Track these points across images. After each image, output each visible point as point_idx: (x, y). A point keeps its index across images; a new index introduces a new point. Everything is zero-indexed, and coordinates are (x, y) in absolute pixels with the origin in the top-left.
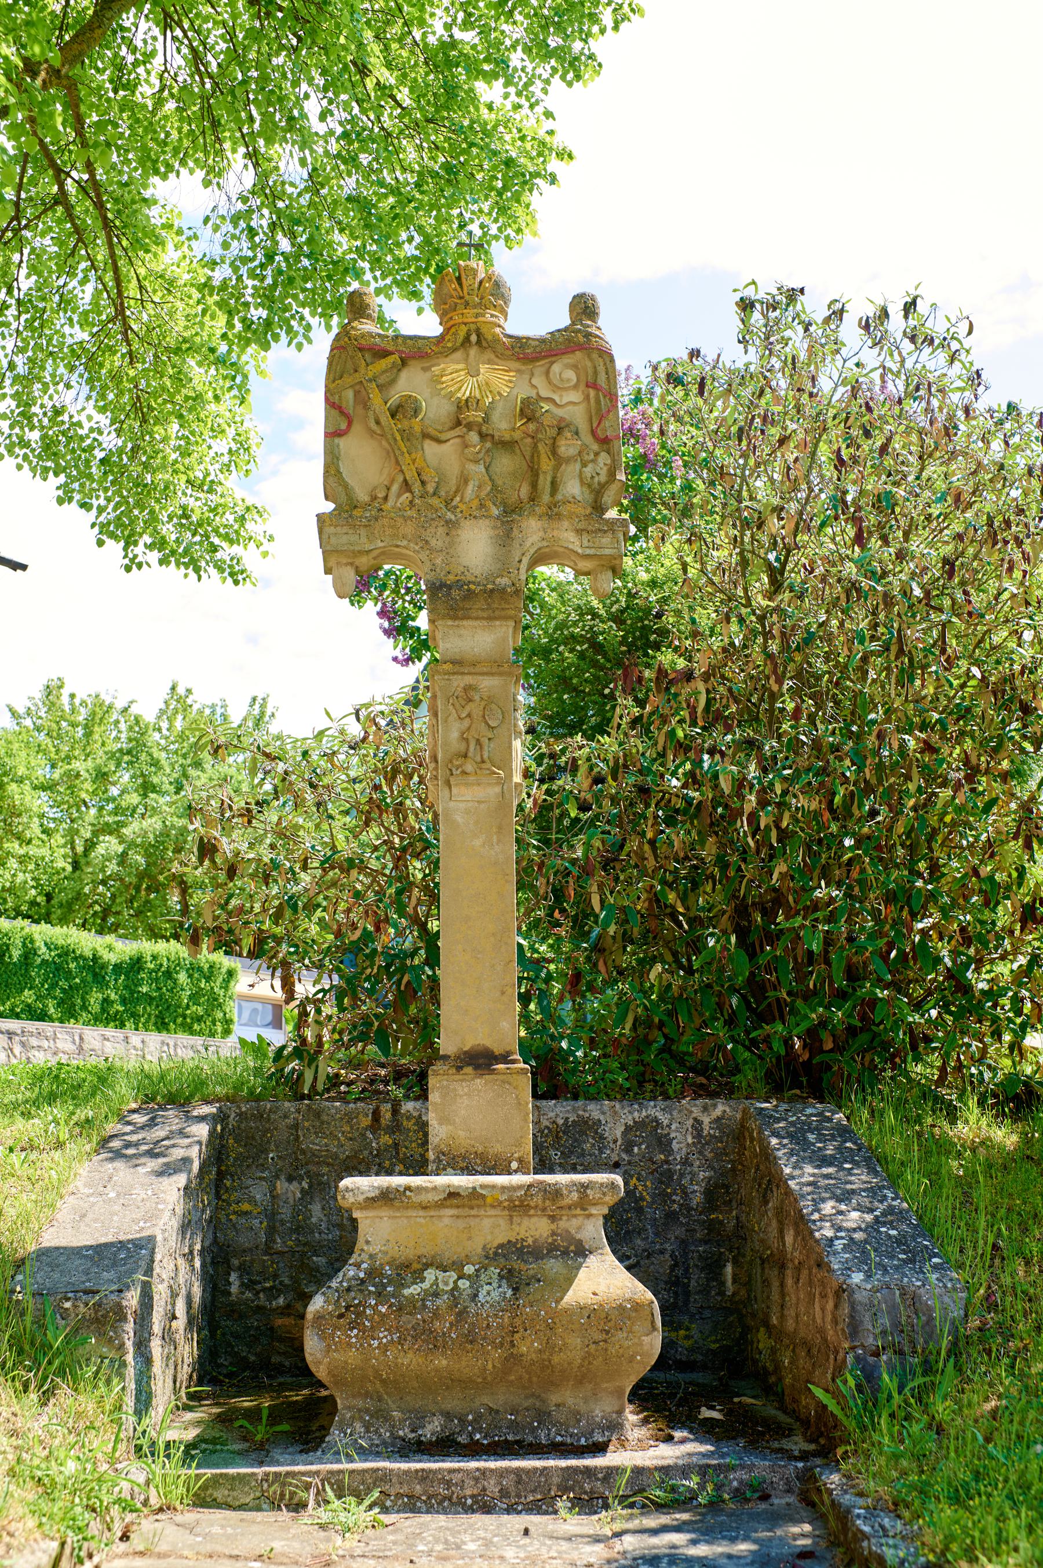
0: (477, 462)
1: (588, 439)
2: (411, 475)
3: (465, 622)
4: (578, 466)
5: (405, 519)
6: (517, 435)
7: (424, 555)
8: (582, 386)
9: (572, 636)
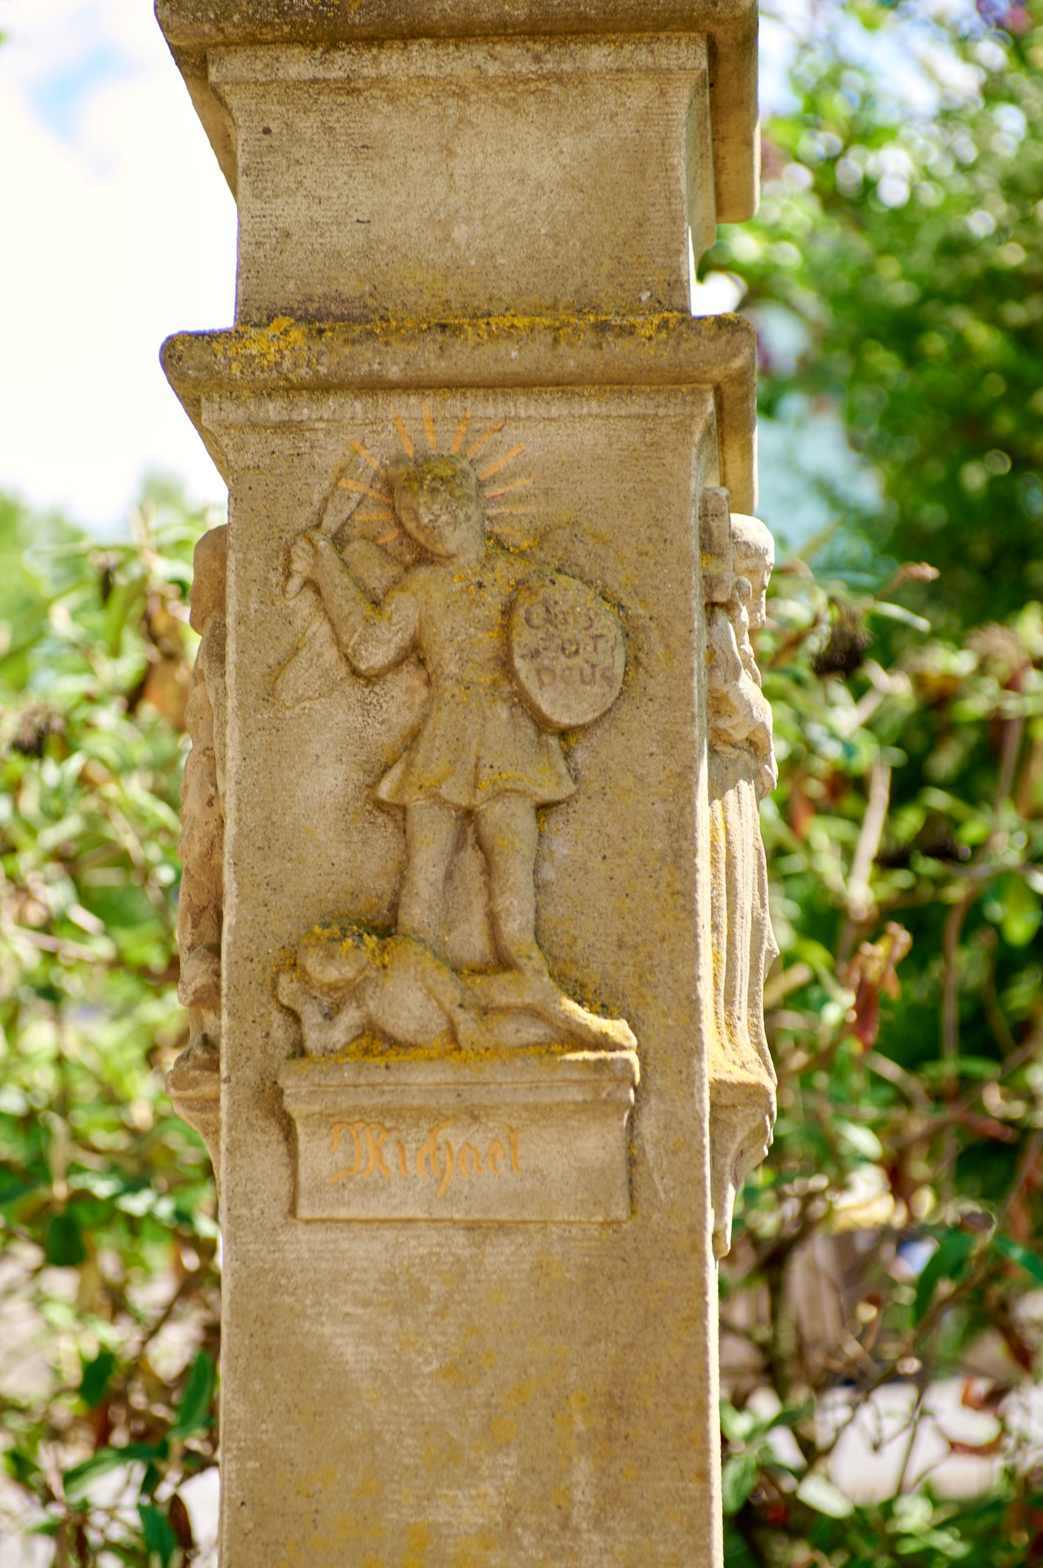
3: (392, 63)
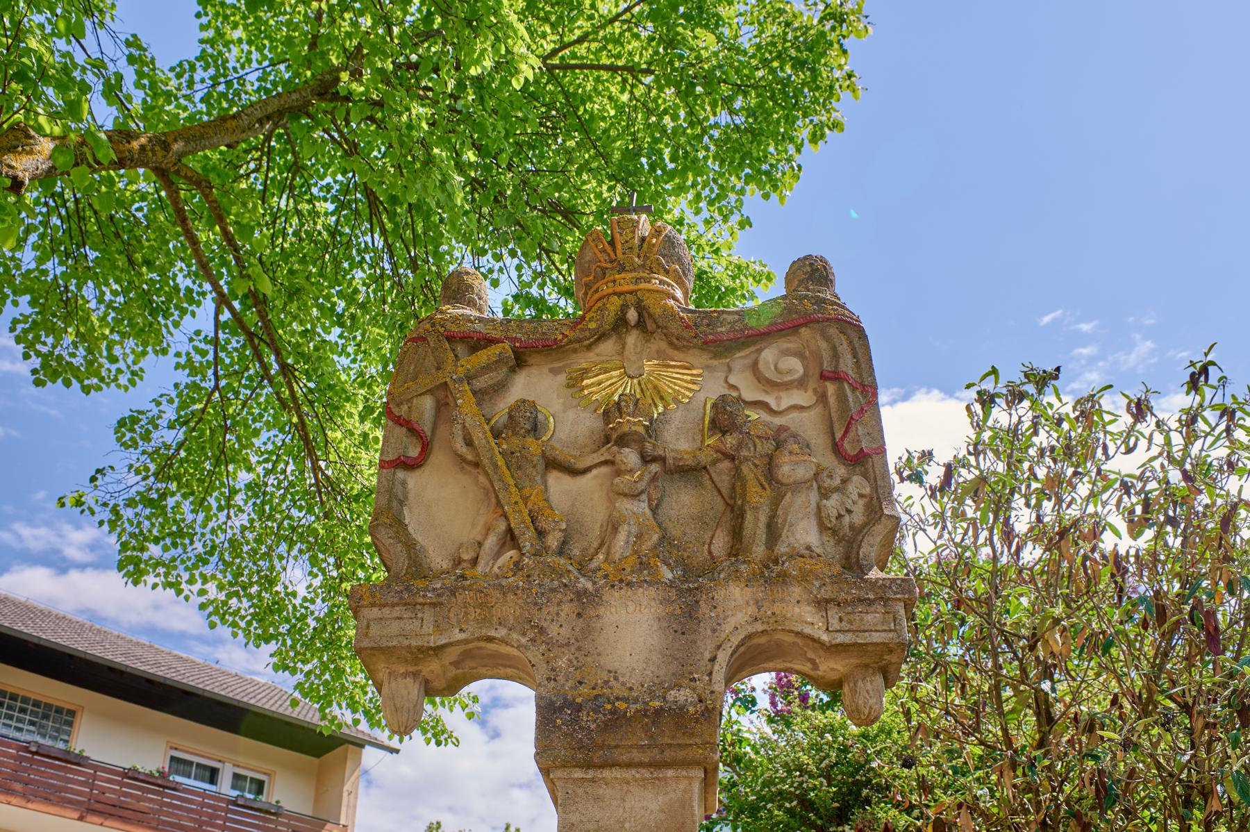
0: (635, 496)
1: (829, 460)
2: (519, 520)
3: (606, 773)
4: (814, 497)
6: (705, 458)
7: (534, 654)
8: (813, 383)
9: (780, 793)
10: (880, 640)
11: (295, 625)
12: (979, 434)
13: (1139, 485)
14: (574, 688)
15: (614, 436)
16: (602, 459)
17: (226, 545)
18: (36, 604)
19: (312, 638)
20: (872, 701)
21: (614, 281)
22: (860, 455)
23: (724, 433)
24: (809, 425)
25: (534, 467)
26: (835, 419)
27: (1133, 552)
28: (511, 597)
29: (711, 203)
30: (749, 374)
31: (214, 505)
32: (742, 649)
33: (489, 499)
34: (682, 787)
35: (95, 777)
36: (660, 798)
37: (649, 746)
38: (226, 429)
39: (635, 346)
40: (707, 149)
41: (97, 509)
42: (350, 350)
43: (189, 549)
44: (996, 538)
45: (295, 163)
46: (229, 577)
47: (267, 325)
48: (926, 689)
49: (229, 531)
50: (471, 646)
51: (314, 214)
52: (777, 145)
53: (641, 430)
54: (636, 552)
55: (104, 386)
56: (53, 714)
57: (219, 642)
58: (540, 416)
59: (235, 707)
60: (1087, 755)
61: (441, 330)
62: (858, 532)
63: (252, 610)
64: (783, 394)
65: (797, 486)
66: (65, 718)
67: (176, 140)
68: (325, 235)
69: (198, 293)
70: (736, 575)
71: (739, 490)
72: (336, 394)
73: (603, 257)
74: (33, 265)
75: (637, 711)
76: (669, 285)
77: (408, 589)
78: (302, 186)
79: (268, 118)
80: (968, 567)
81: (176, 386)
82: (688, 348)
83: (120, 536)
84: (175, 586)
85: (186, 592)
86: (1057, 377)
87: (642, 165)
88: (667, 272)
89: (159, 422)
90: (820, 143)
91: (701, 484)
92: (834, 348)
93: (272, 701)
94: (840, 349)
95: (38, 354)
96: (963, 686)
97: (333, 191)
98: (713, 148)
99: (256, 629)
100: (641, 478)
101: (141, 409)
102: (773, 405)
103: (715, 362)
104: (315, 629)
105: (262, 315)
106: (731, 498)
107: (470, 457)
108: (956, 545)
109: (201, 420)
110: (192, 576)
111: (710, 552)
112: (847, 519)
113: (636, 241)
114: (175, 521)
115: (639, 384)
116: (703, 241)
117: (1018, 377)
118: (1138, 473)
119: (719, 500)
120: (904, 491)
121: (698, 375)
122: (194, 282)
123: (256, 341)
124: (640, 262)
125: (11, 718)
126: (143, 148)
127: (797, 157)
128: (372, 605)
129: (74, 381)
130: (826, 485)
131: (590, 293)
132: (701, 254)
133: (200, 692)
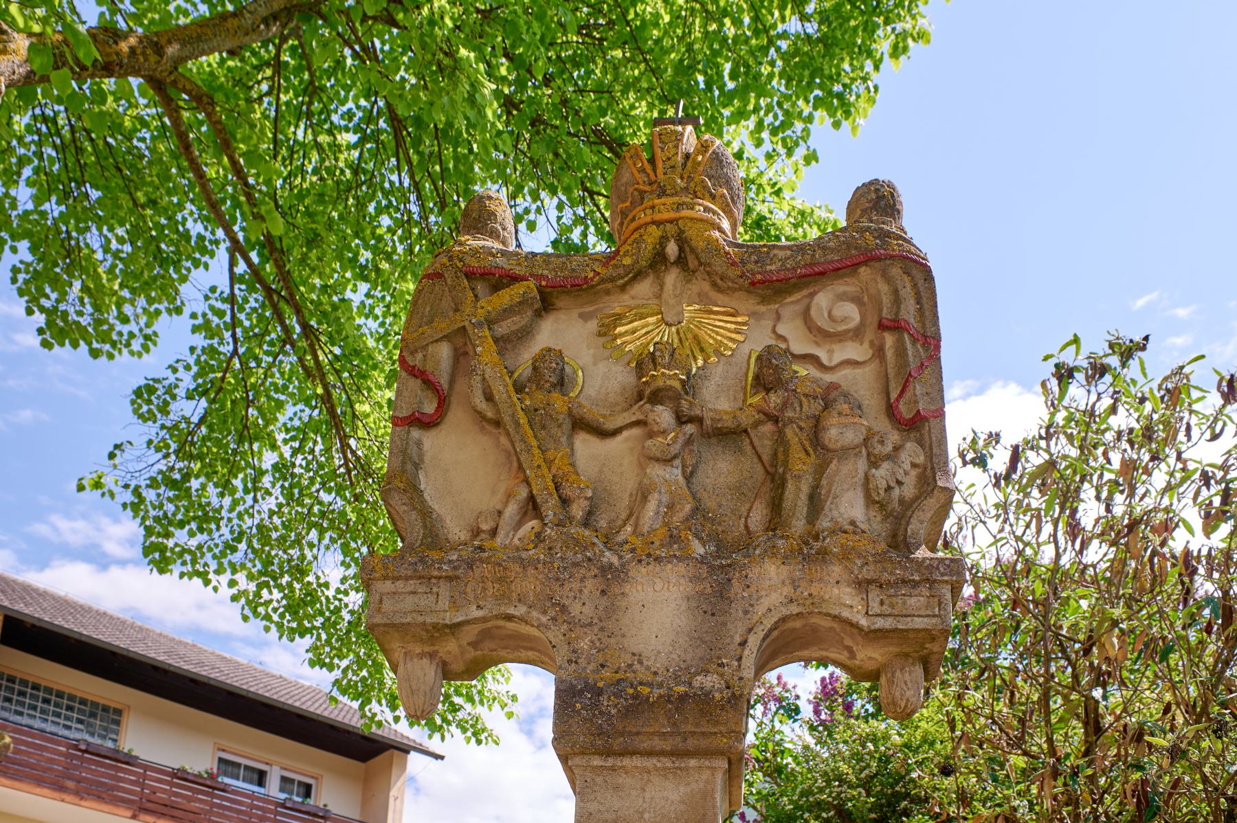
0: (668, 461)
1: (882, 424)
2: (542, 486)
3: (627, 762)
4: (862, 465)
5: (524, 564)
6: (746, 419)
7: (555, 635)
8: (870, 334)
9: (819, 804)
10: (922, 626)
11: (329, 619)
12: (1053, 415)
13: (1220, 474)
14: (596, 671)
15: (647, 392)
16: (634, 419)
17: (254, 530)
18: (76, 599)
19: (349, 632)
20: (909, 693)
21: (653, 207)
22: (919, 422)
23: (768, 390)
24: (862, 383)
25: (560, 426)
26: (891, 376)
27: (1204, 552)
28: (531, 571)
29: (774, 131)
30: (799, 322)
31: (240, 487)
32: (775, 633)
33: (511, 462)
34: (704, 777)
35: (145, 777)
36: (682, 789)
37: (671, 734)
38: (249, 403)
39: (675, 286)
40: (772, 64)
41: (117, 490)
42: (378, 311)
43: (216, 535)
44: (1060, 534)
45: (311, 82)
46: (259, 566)
47: (284, 276)
48: (974, 697)
49: (256, 515)
50: (489, 624)
51: (336, 148)
52: (852, 59)
53: (677, 385)
54: (666, 524)
55: (116, 353)
56: (100, 712)
57: (261, 645)
58: (568, 369)
59: (280, 709)
60: (1132, 766)
61: (460, 265)
62: (908, 506)
63: (284, 602)
64: (836, 347)
65: (845, 452)
66: (113, 717)
67: (169, 42)
68: (348, 173)
69: (210, 241)
70: (772, 552)
71: (781, 457)
72: (363, 361)
73: (641, 178)
74: (30, 206)
75: (661, 696)
76: (714, 213)
77: (422, 560)
78: (321, 113)
79: (275, 17)
80: (1029, 565)
81: (192, 349)
82: (734, 290)
83: (144, 519)
84: (204, 576)
85: (214, 583)
86: (1144, 348)
87: (697, 83)
88: (713, 197)
89: (176, 391)
90: (903, 58)
91: (741, 451)
92: (896, 292)
93: (317, 705)
94: (902, 293)
95: (42, 309)
96: (1012, 694)
97: (356, 119)
98: (779, 63)
99: (289, 621)
100: (675, 440)
101: (156, 377)
102: (825, 361)
103: (763, 308)
104: (349, 622)
105: (280, 266)
106: (772, 466)
107: (490, 414)
108: (1018, 539)
109: (220, 389)
110: (220, 565)
111: (747, 527)
112: (896, 492)
113: (679, 158)
114: (200, 505)
115: (678, 332)
116: (764, 181)
117: (1101, 348)
118: (1219, 461)
119: (759, 467)
120: (966, 477)
121: (744, 324)
122: (206, 229)
123: (275, 298)
124: (683, 185)
125: (59, 715)
126: (132, 50)
127: (874, 75)
128: (385, 578)
129: (82, 343)
130: (876, 452)
131: (626, 222)
132: (761, 197)
133: (244, 693)
